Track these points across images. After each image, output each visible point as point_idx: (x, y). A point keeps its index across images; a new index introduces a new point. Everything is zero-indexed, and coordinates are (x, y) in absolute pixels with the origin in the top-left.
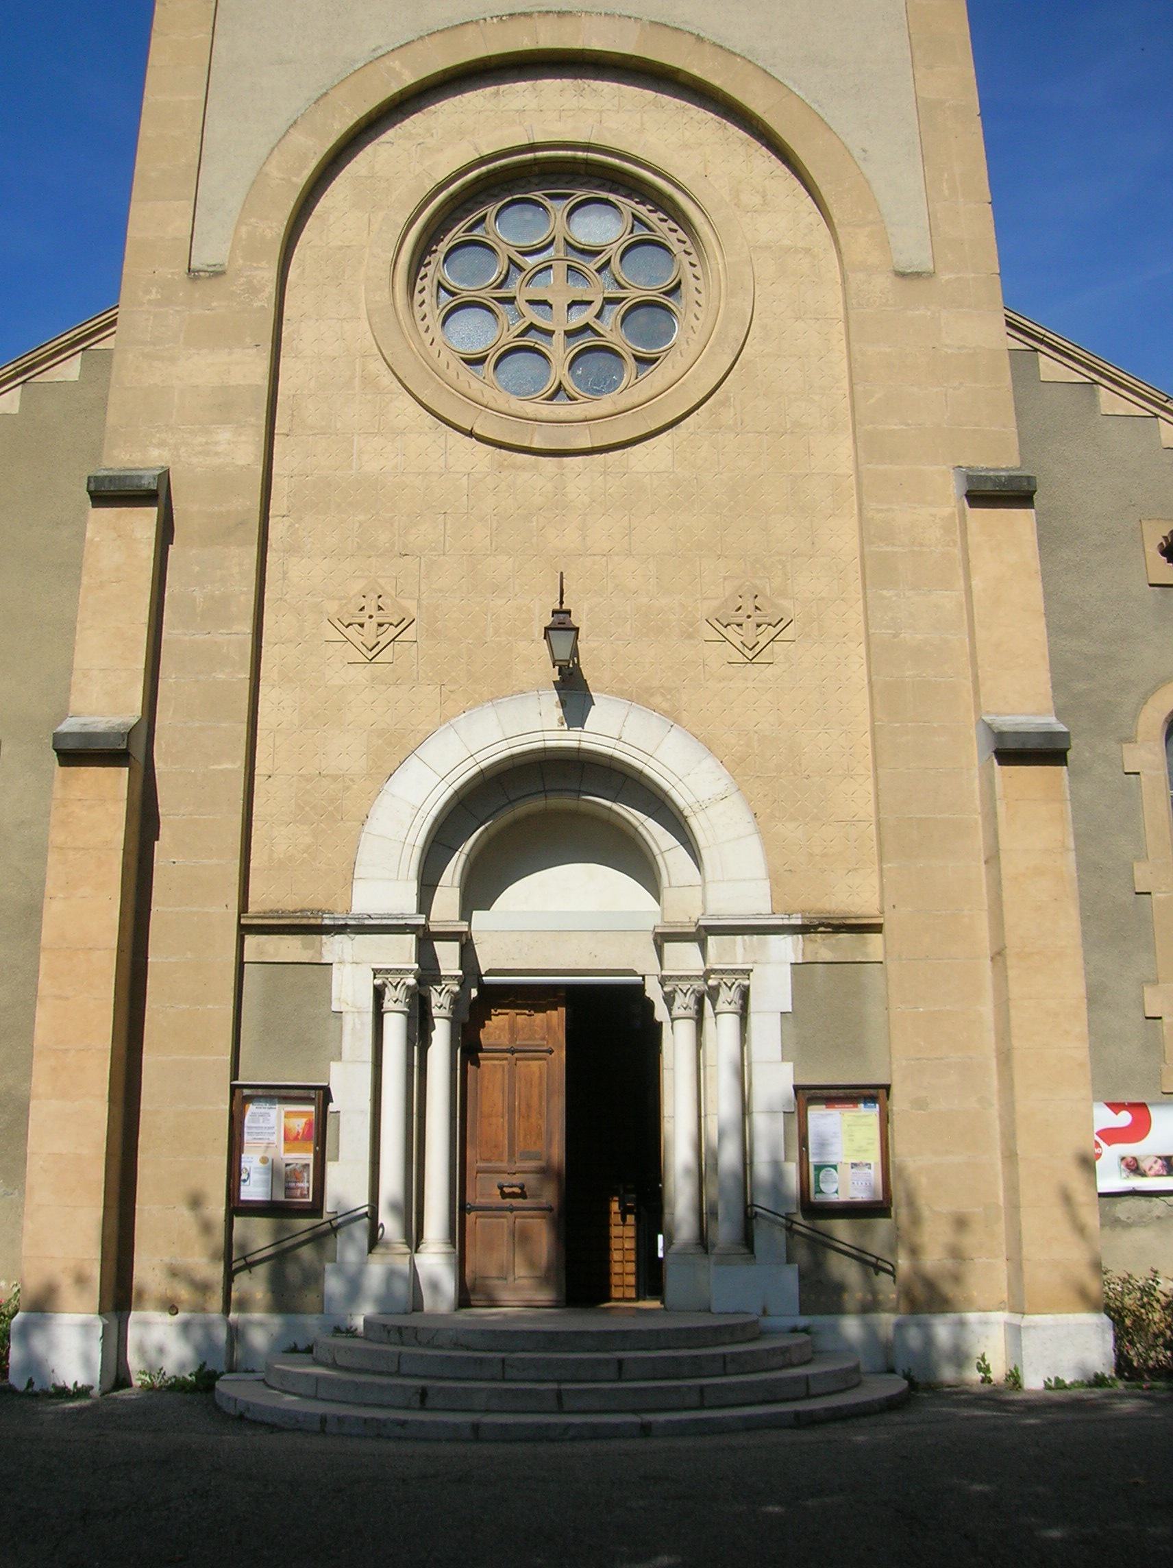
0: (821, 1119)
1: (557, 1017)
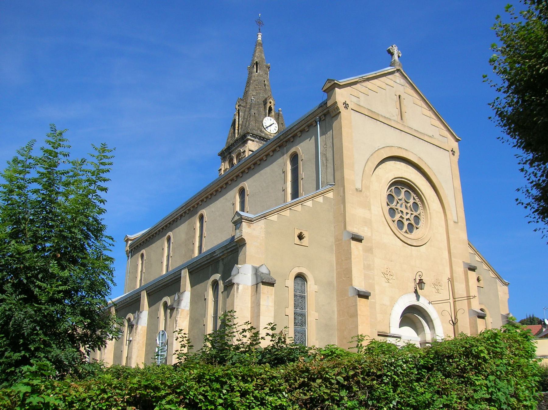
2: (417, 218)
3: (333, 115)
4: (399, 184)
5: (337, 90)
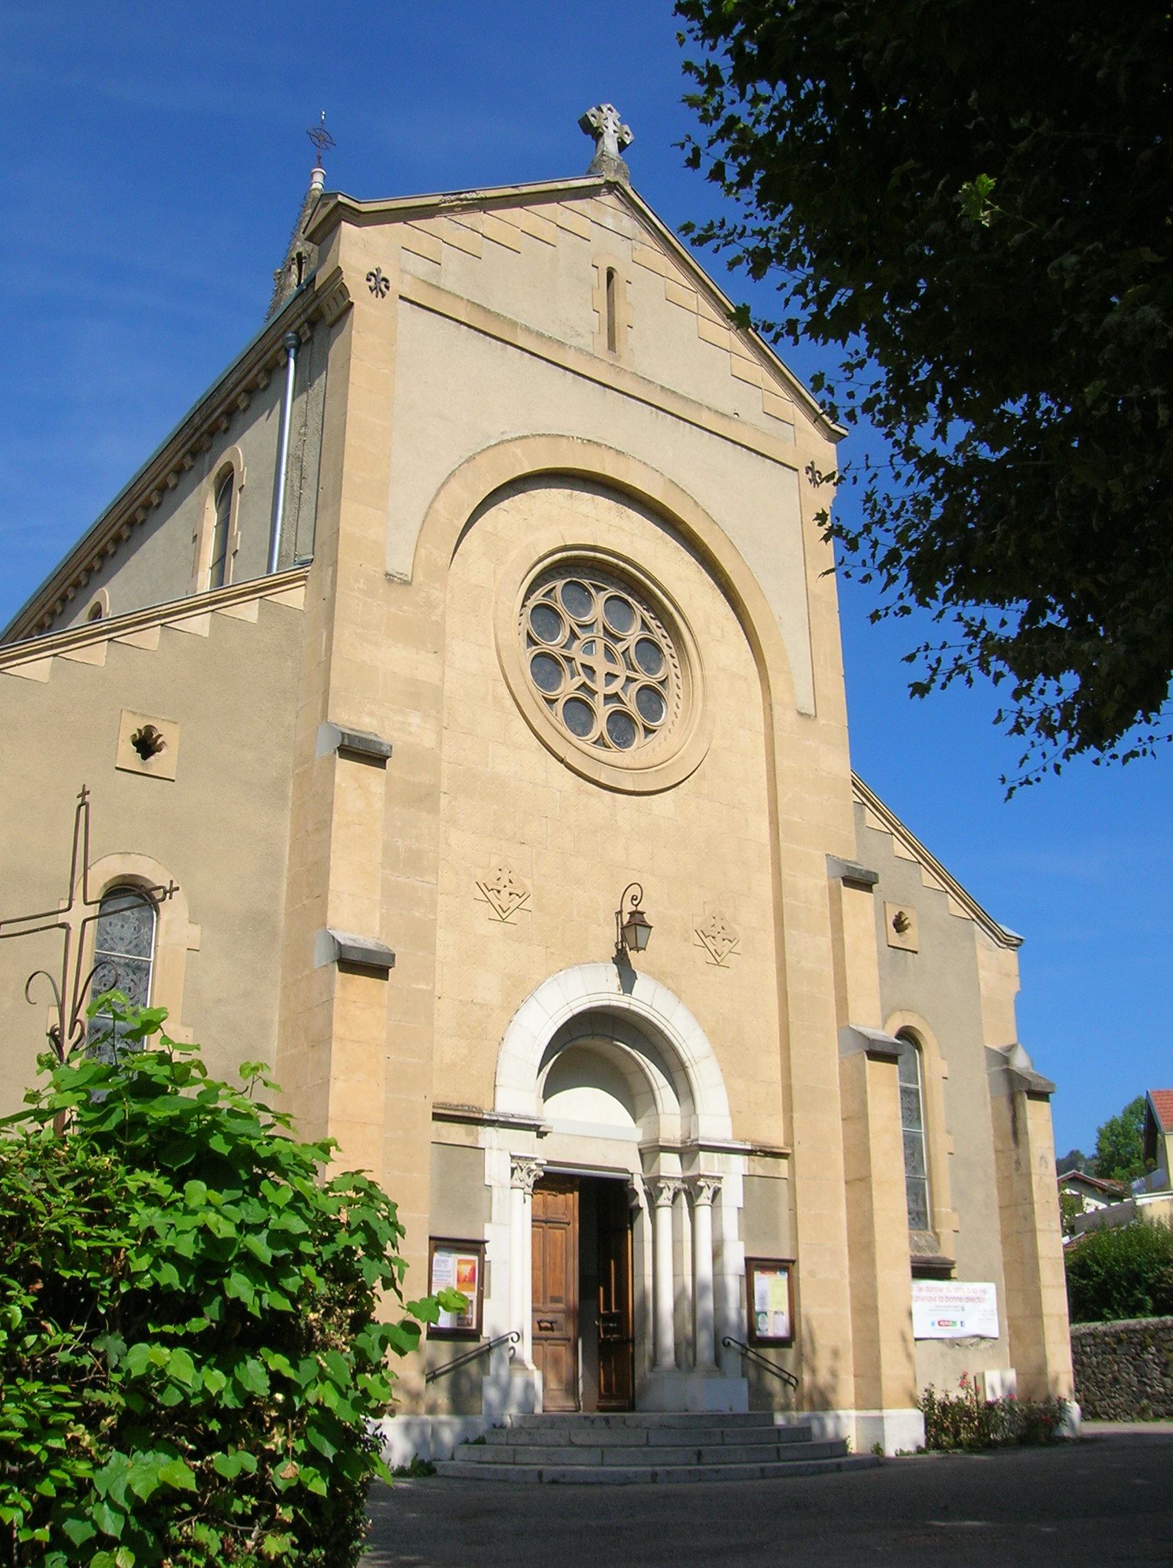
0: (763, 1281)
1: (573, 1198)
2: (652, 698)
3: (330, 318)
4: (579, 570)
5: (345, 226)
